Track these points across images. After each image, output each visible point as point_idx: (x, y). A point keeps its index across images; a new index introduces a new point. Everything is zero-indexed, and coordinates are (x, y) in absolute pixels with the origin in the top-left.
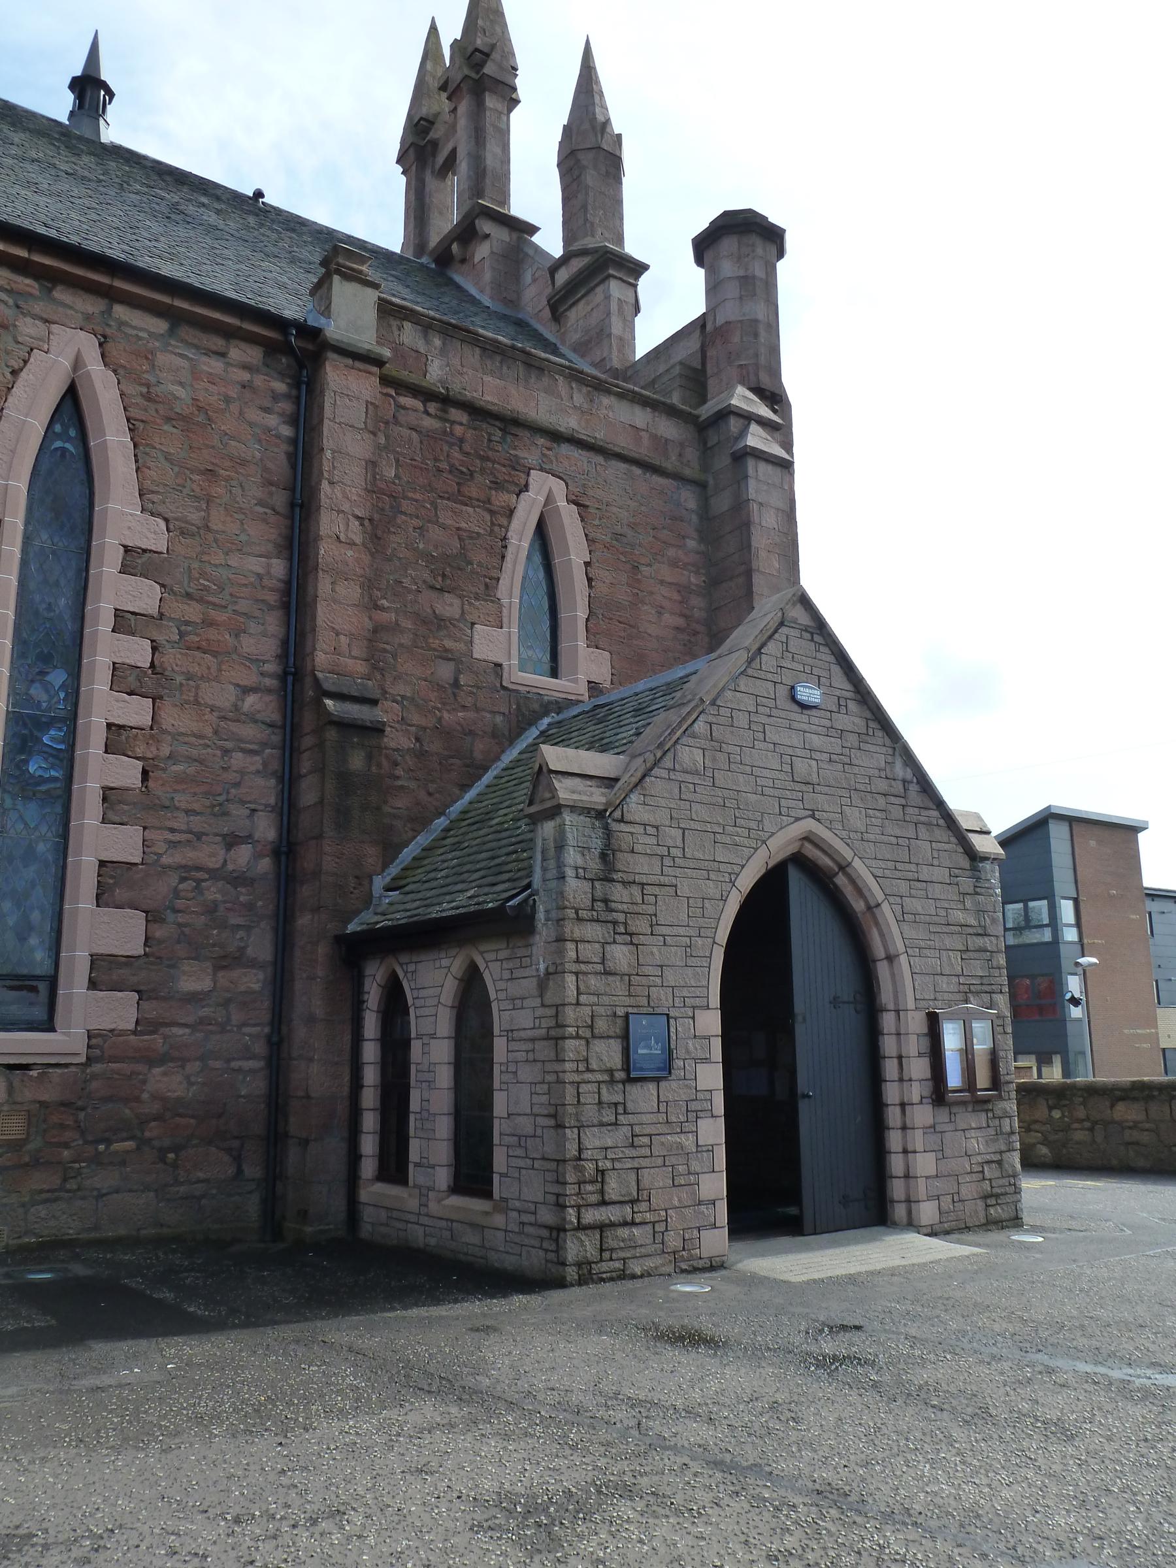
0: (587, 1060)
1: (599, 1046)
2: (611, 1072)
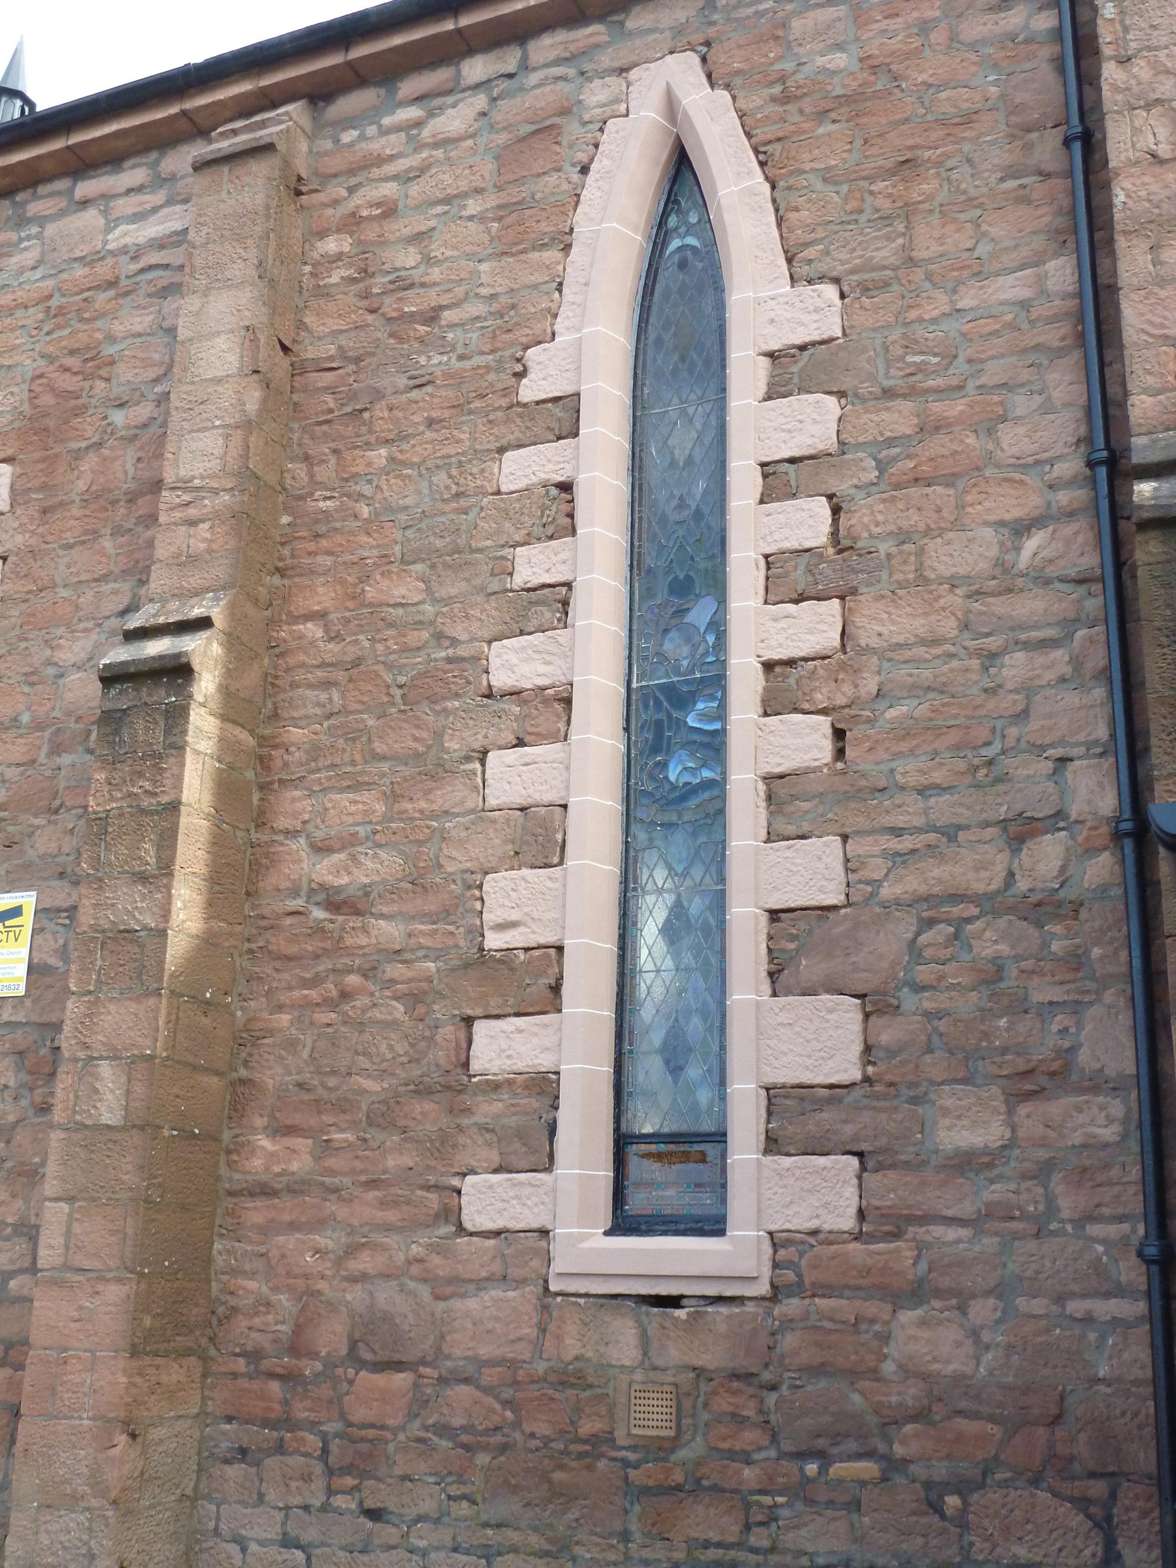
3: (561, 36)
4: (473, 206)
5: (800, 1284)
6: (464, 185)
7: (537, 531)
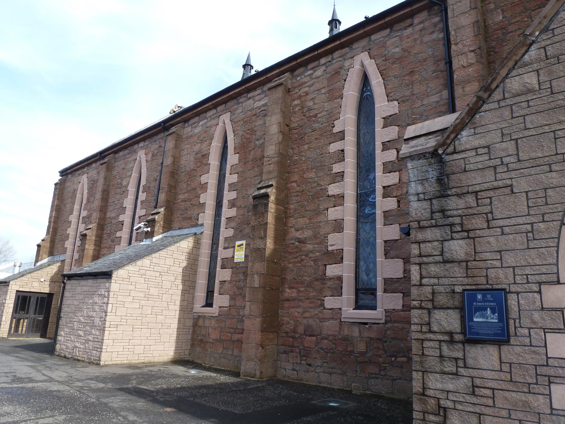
0: (429, 324)
1: (438, 315)
2: (451, 334)
3: (340, 51)
4: (323, 91)
5: (391, 320)
6: (321, 87)
7: (337, 161)
